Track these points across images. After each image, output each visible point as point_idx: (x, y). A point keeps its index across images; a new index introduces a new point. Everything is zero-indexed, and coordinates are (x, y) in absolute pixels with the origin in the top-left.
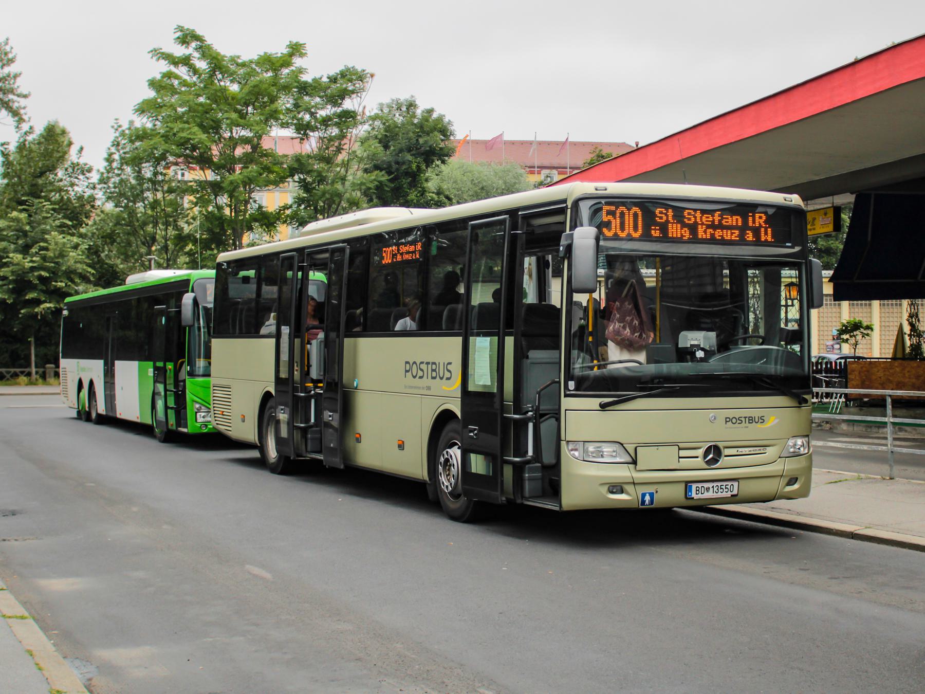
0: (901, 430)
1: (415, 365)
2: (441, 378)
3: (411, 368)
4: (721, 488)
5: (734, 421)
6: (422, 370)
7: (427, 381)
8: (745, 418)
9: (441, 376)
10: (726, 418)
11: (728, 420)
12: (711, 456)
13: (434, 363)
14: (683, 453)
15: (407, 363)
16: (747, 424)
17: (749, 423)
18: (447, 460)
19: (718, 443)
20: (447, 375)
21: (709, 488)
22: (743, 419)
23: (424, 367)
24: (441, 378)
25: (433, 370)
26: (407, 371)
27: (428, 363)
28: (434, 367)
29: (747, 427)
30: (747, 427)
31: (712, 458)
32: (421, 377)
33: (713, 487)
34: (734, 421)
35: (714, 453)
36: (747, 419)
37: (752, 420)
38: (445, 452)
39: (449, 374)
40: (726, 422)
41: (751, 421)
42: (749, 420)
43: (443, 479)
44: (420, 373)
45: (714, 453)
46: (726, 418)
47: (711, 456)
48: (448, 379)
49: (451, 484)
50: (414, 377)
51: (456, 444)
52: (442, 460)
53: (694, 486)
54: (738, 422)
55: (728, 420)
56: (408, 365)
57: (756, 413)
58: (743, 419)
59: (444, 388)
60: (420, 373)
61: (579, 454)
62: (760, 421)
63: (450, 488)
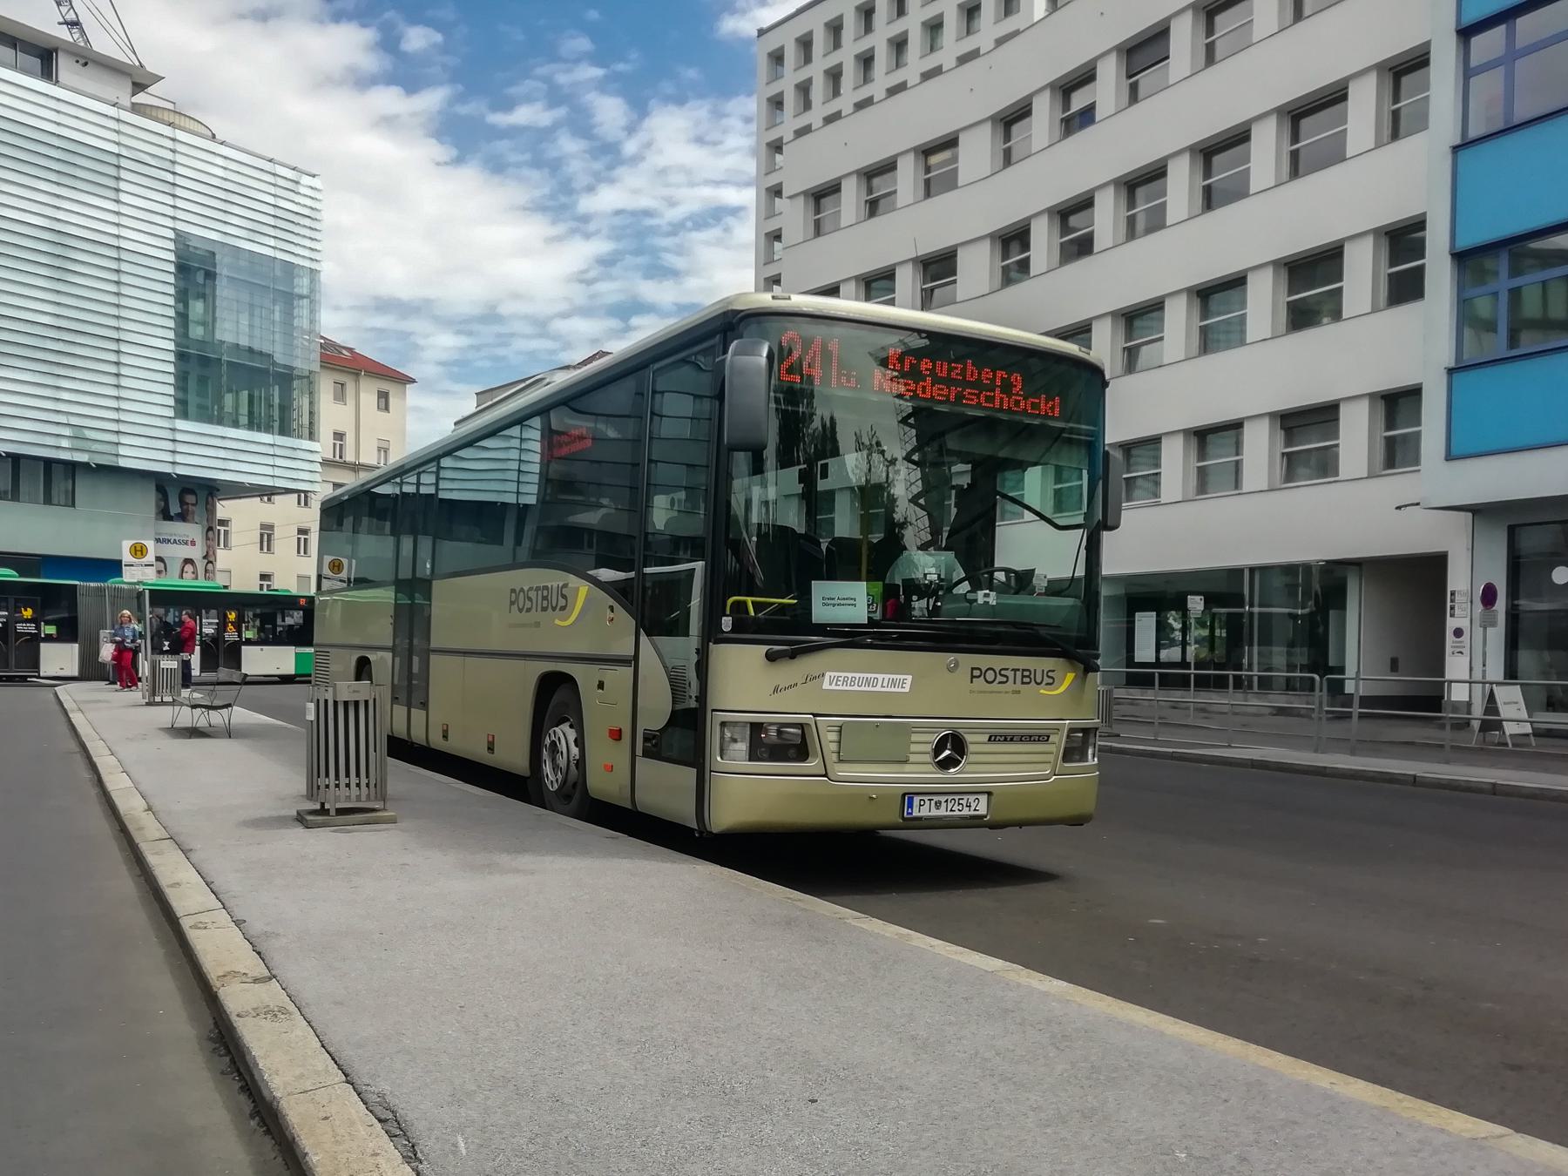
0: (577, 765)
1: (522, 593)
2: (554, 609)
3: (517, 598)
4: (959, 804)
5: (990, 675)
6: (530, 599)
7: (536, 615)
8: (1015, 670)
9: (189, 568)
10: (973, 669)
11: (976, 673)
12: (947, 752)
13: (546, 588)
14: (852, 602)
15: (513, 591)
16: (1019, 686)
17: (1023, 683)
18: (553, 743)
19: (959, 730)
20: (562, 602)
21: (940, 802)
22: (1010, 674)
23: (532, 594)
24: (554, 609)
25: (545, 598)
26: (512, 603)
27: (538, 589)
28: (545, 593)
29: (1019, 692)
30: (1019, 692)
31: (947, 757)
32: (529, 610)
33: (947, 801)
34: (990, 675)
35: (952, 748)
36: (1019, 674)
37: (1028, 677)
38: (551, 731)
39: (564, 601)
40: (973, 677)
41: (1026, 673)
42: (1023, 676)
43: (547, 769)
44: (528, 604)
45: (952, 748)
46: (973, 669)
47: (947, 752)
48: (563, 608)
49: (557, 779)
50: (520, 610)
51: (568, 720)
52: (547, 741)
53: (916, 800)
54: (1000, 678)
55: (976, 673)
56: (513, 595)
57: (635, 602)
58: (1010, 674)
59: (557, 622)
60: (528, 604)
61: (827, 738)
62: (1047, 680)
63: (556, 786)
